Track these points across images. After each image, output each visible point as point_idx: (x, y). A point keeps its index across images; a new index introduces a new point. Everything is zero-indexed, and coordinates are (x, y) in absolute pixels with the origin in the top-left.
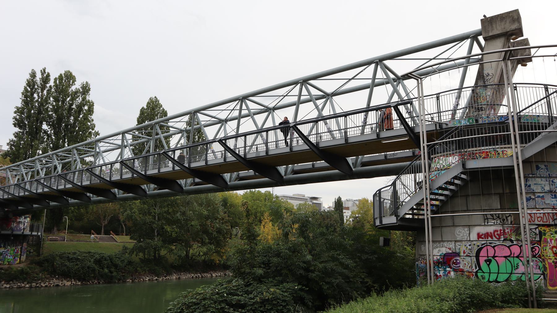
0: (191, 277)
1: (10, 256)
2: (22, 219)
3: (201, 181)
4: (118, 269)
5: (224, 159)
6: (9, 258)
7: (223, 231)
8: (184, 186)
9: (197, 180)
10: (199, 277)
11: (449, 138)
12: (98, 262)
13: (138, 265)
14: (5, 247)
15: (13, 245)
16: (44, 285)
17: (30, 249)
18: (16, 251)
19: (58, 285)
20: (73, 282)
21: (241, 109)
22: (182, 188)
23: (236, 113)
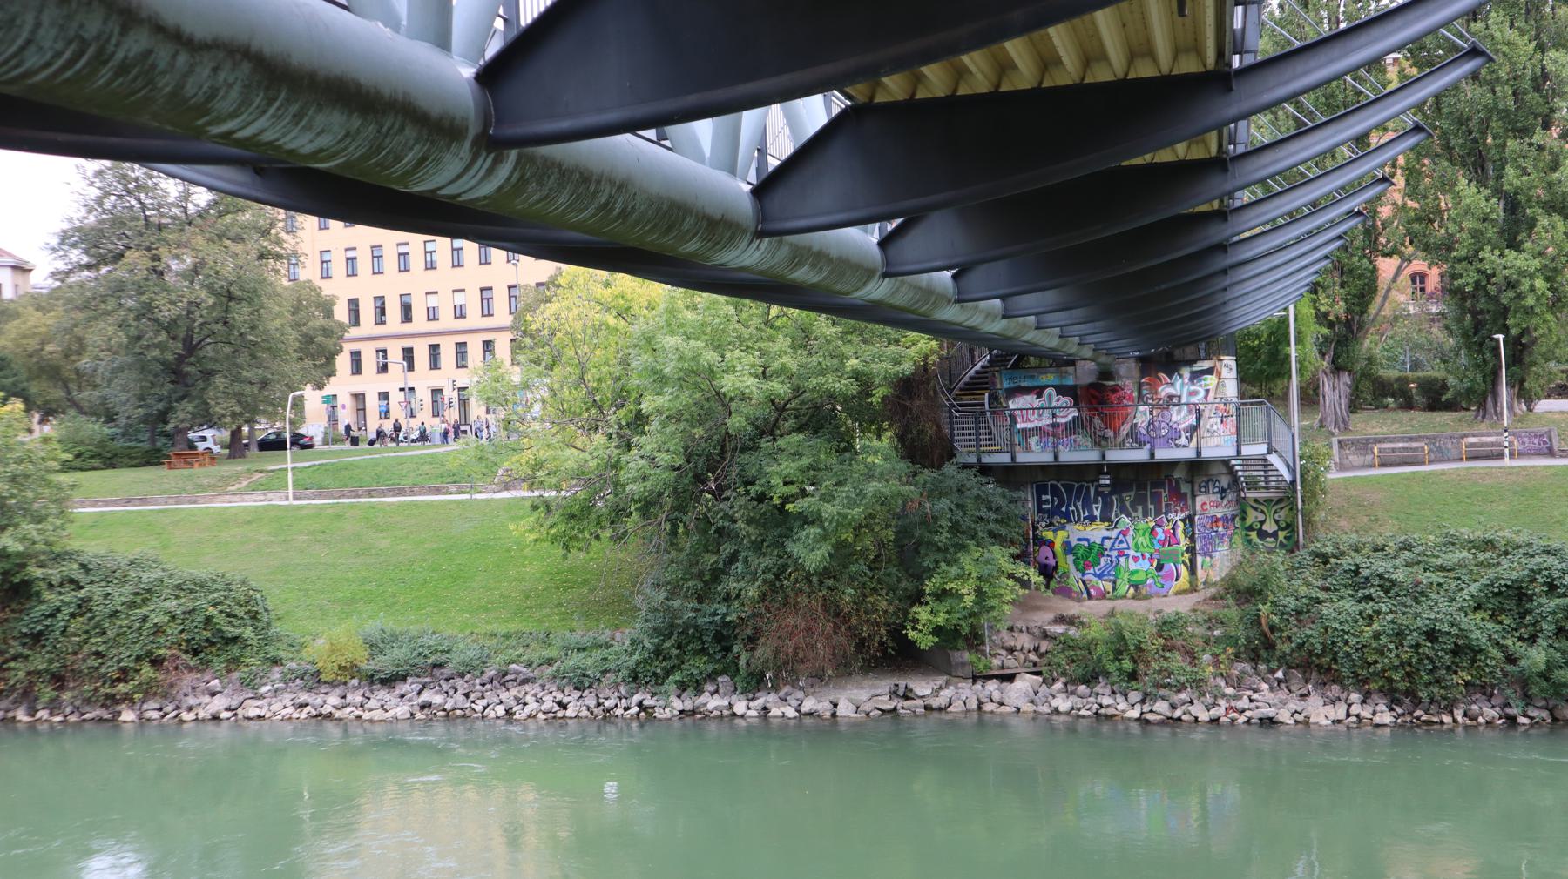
1: (1136, 559)
2: (1183, 385)
3: (902, 219)
6: (1133, 566)
14: (1109, 520)
15: (1140, 508)
16: (1204, 716)
17: (1261, 517)
18: (1161, 536)
19: (1269, 723)
20: (1355, 709)
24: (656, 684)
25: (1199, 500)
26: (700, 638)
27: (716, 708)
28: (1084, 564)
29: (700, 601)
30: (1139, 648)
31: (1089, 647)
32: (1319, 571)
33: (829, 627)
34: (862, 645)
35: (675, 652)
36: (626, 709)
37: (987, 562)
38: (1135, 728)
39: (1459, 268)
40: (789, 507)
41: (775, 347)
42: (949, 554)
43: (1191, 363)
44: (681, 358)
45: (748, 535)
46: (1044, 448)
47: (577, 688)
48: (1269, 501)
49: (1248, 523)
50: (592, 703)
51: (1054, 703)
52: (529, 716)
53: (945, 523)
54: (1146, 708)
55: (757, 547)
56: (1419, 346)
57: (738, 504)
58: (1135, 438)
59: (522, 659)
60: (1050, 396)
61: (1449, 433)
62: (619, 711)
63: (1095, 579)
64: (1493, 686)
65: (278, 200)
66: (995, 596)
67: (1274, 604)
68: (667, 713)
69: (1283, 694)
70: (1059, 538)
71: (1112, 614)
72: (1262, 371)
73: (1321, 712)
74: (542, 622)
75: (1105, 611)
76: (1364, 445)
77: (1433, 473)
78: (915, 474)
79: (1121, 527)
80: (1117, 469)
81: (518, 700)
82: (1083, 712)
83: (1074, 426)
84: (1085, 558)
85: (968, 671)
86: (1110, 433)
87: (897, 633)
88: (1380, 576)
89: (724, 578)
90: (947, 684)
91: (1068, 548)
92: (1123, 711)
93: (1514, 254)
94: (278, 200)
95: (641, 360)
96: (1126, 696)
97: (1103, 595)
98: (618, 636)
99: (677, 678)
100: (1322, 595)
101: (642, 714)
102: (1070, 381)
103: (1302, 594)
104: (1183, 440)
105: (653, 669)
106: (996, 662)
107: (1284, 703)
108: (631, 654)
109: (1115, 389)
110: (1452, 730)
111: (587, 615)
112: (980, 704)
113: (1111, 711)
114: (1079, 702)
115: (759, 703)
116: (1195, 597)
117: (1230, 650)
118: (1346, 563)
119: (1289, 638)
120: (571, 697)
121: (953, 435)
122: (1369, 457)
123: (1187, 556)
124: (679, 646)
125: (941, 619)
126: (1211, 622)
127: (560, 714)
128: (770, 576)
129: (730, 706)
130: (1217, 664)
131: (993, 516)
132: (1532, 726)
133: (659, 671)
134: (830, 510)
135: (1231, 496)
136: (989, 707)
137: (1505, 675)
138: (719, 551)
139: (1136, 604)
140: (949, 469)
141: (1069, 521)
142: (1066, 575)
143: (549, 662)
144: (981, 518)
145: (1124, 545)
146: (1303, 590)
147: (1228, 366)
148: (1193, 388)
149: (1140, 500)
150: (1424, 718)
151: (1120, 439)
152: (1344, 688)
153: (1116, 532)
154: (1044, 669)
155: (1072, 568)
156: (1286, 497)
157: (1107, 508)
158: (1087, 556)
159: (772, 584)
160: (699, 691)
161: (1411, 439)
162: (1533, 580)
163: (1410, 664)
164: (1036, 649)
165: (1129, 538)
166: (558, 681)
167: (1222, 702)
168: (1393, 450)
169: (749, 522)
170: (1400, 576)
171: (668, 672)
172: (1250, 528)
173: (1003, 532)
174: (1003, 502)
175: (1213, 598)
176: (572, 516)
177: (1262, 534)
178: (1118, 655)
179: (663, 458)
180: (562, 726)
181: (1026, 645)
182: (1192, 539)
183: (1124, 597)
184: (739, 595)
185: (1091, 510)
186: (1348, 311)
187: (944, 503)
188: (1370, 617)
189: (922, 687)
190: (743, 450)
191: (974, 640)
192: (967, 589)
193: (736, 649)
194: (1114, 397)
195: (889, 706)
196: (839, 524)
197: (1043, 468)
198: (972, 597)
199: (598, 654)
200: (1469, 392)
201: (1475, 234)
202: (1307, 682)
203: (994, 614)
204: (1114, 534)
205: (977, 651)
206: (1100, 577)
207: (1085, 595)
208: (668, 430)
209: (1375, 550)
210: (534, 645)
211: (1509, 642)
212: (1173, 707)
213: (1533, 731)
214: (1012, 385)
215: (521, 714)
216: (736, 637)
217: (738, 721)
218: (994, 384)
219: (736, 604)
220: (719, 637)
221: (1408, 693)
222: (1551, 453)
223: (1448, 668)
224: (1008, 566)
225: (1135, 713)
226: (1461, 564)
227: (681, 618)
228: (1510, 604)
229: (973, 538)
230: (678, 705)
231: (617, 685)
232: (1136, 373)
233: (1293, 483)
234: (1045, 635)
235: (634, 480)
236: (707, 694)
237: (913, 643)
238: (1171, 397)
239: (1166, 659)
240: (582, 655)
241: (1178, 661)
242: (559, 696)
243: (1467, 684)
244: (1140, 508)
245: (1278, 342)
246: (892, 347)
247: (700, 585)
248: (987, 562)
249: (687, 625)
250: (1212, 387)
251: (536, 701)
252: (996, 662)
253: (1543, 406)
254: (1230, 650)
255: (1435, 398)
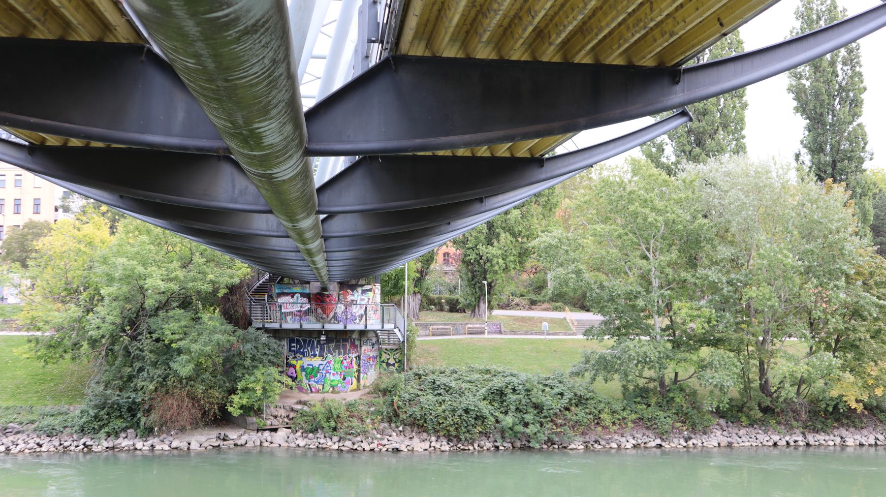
0: (771, 443)
1: (334, 375)
4: (545, 417)
6: (332, 378)
7: (869, 311)
10: (796, 447)
12: (498, 395)
13: (602, 405)
14: (323, 356)
15: (337, 351)
16: (367, 448)
17: (388, 357)
18: (346, 364)
19: (397, 450)
20: (433, 444)
24: (94, 433)
25: (363, 348)
26: (119, 410)
27: (126, 446)
28: (310, 376)
29: (121, 390)
30: (338, 417)
31: (314, 416)
32: (417, 381)
33: (190, 405)
34: (205, 413)
35: (106, 417)
36: (77, 446)
37: (269, 375)
38: (335, 455)
39: (468, 252)
40: (173, 345)
41: (172, 266)
42: (250, 370)
43: (362, 286)
44: (125, 269)
45: (150, 358)
46: (294, 322)
47: (48, 436)
48: (392, 349)
49: (382, 359)
50: (57, 443)
51: (297, 442)
52: (20, 451)
53: (249, 355)
54: (341, 444)
55: (155, 364)
56: (441, 285)
57: (146, 343)
58: (336, 319)
59: (16, 420)
60: (297, 297)
61: (461, 322)
62: (72, 448)
63: (314, 384)
64: (490, 433)
65: (41, 170)
66: (271, 391)
67: (400, 396)
68: (100, 448)
69: (402, 437)
70: (299, 364)
71: (323, 400)
72: (390, 292)
73: (419, 445)
74: (27, 401)
75: (320, 399)
76: (425, 326)
77: (457, 339)
78: (235, 331)
79: (328, 360)
80: (328, 332)
81: (13, 442)
82: (311, 446)
83: (309, 312)
84: (310, 374)
85: (255, 427)
86: (325, 316)
87: (223, 409)
88: (445, 385)
89: (135, 380)
90: (245, 433)
91: (303, 369)
92: (330, 446)
93: (491, 248)
94: (41, 170)
95: (100, 269)
96: (331, 439)
97: (318, 391)
98: (72, 408)
99: (106, 430)
100: (420, 393)
101: (85, 449)
102: (307, 291)
103: (411, 392)
104: (357, 321)
105: (93, 426)
106: (269, 422)
107: (403, 441)
108: (81, 417)
109: (328, 296)
110: (473, 453)
111: (53, 398)
112: (261, 442)
113: (324, 446)
114: (309, 442)
115: (149, 443)
116: (359, 393)
117: (379, 418)
118: (430, 378)
119: (406, 412)
120: (45, 441)
121: (251, 313)
122: (428, 332)
123: (356, 374)
124: (108, 414)
125: (244, 402)
126: (371, 404)
127: (38, 450)
128: (160, 379)
129: (134, 445)
130: (373, 424)
131: (272, 353)
132: (505, 450)
133: (96, 427)
134: (195, 347)
135: (376, 347)
136: (266, 444)
137: (495, 428)
138: (132, 366)
139: (334, 396)
140: (251, 330)
141: (304, 356)
142: (301, 381)
143: (33, 422)
144: (265, 354)
145: (329, 368)
146: (412, 391)
147: (378, 288)
148: (362, 297)
149: (337, 347)
150: (462, 447)
151: (329, 319)
152: (429, 435)
153: (325, 362)
154: (292, 426)
155: (304, 378)
156: (399, 348)
157: (322, 350)
158: (311, 373)
159: (161, 383)
160: (117, 436)
161: (445, 324)
162: (507, 387)
163: (457, 424)
164: (288, 417)
165: (331, 365)
166: (37, 432)
167: (376, 441)
168: (438, 329)
169: (151, 352)
170: (453, 384)
171: (101, 428)
172: (383, 362)
173: (275, 360)
174: (275, 346)
175: (369, 393)
176: (50, 346)
177: (388, 364)
178: (328, 420)
179: (110, 319)
180: (38, 456)
181: (283, 415)
182: (359, 366)
183: (328, 392)
184: (142, 389)
185: (314, 352)
186: (423, 267)
187: (249, 346)
188: (441, 403)
189: (233, 434)
190: (150, 316)
191: (259, 412)
192: (258, 387)
193: (139, 415)
194: (328, 300)
195: (216, 444)
196: (200, 354)
197: (293, 331)
198: (261, 392)
199: (61, 418)
200: (469, 305)
201: (476, 238)
202: (412, 431)
203: (270, 399)
204: (324, 363)
205: (259, 417)
206: (317, 382)
207: (309, 391)
208: (113, 305)
209: (441, 373)
210: (23, 413)
211: (497, 414)
212: (354, 444)
213: (505, 453)
214: (280, 291)
215: (14, 450)
216: (139, 410)
217: (138, 452)
218: (271, 290)
219: (140, 393)
220: (130, 410)
221: (455, 437)
222: (500, 332)
223: (473, 425)
224: (278, 377)
225: (336, 447)
226: (477, 380)
227: (110, 399)
228: (497, 398)
229: (261, 363)
230: (105, 444)
231: (72, 434)
232: (337, 289)
233: (403, 342)
234: (292, 410)
235: (93, 329)
236: (121, 438)
237: (230, 413)
238: (353, 301)
239: (350, 421)
240: (52, 418)
241: (355, 422)
242: (38, 440)
243: (480, 432)
244: (337, 351)
245: (399, 279)
246: (229, 270)
247: (121, 383)
248: (269, 375)
249: (113, 403)
250: (371, 298)
251: (24, 443)
252: (269, 422)
253: (497, 312)
254: (379, 418)
255: (454, 307)
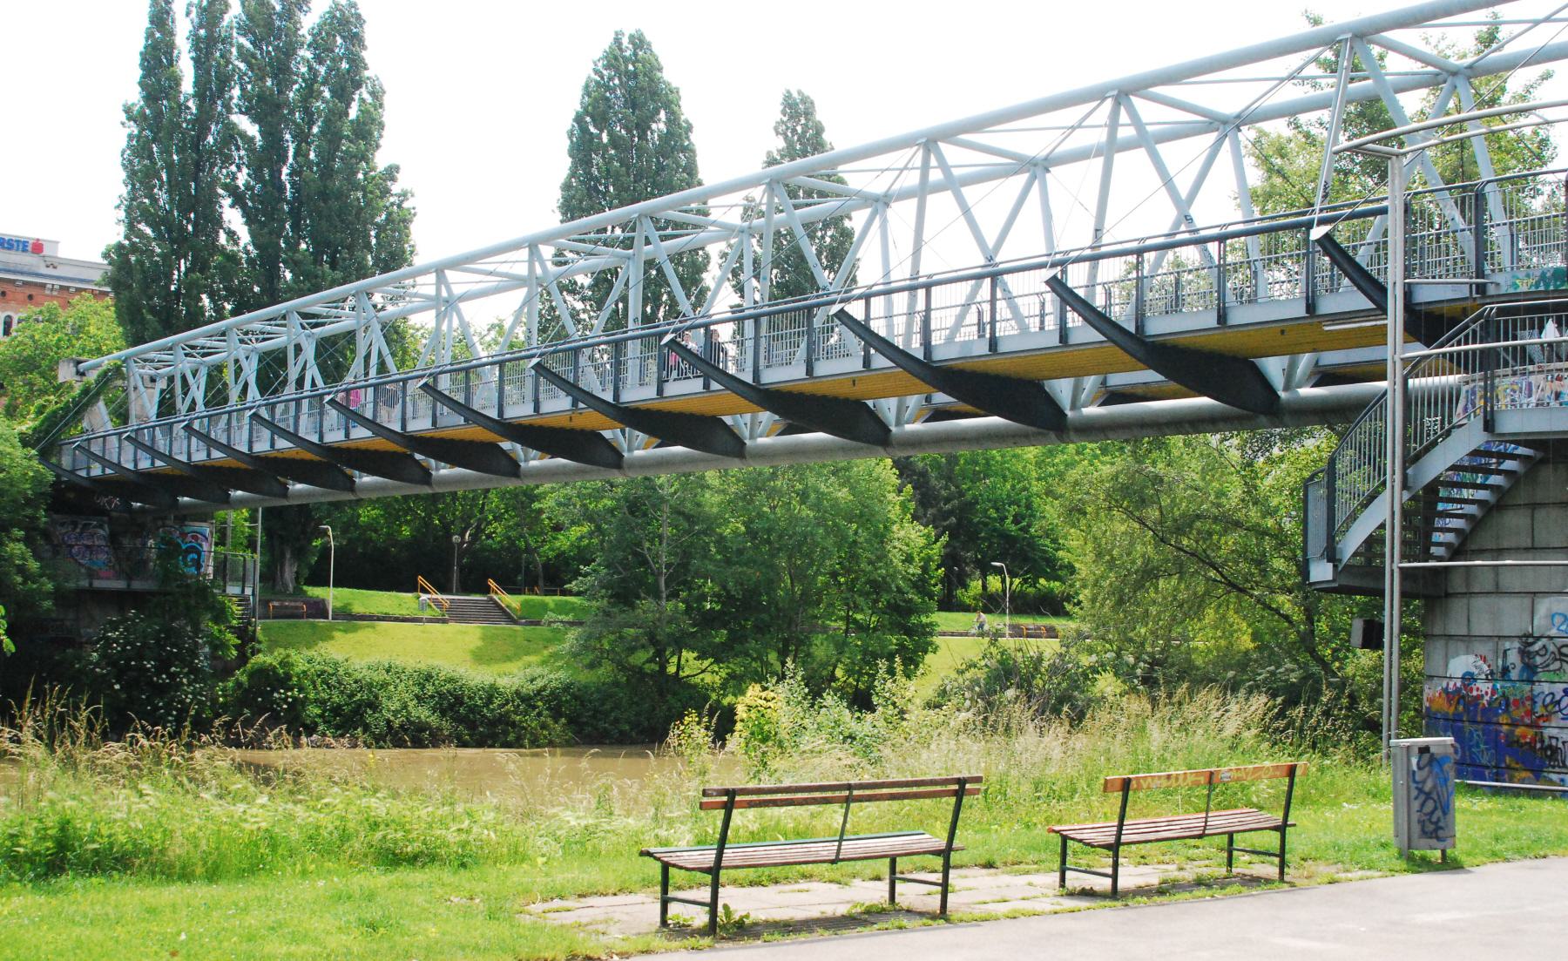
3: (951, 399)
5: (990, 345)
8: (746, 433)
9: (941, 398)
11: (1459, 344)
21: (925, 168)
22: (741, 443)
23: (912, 179)
